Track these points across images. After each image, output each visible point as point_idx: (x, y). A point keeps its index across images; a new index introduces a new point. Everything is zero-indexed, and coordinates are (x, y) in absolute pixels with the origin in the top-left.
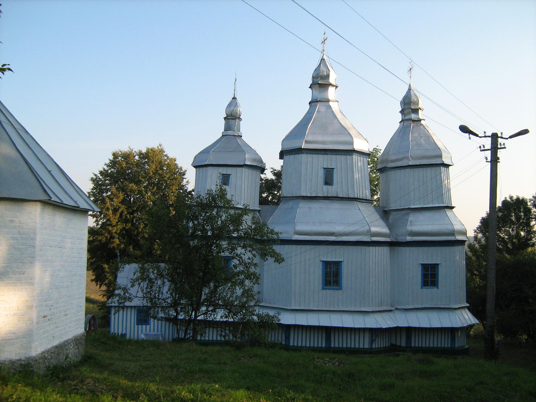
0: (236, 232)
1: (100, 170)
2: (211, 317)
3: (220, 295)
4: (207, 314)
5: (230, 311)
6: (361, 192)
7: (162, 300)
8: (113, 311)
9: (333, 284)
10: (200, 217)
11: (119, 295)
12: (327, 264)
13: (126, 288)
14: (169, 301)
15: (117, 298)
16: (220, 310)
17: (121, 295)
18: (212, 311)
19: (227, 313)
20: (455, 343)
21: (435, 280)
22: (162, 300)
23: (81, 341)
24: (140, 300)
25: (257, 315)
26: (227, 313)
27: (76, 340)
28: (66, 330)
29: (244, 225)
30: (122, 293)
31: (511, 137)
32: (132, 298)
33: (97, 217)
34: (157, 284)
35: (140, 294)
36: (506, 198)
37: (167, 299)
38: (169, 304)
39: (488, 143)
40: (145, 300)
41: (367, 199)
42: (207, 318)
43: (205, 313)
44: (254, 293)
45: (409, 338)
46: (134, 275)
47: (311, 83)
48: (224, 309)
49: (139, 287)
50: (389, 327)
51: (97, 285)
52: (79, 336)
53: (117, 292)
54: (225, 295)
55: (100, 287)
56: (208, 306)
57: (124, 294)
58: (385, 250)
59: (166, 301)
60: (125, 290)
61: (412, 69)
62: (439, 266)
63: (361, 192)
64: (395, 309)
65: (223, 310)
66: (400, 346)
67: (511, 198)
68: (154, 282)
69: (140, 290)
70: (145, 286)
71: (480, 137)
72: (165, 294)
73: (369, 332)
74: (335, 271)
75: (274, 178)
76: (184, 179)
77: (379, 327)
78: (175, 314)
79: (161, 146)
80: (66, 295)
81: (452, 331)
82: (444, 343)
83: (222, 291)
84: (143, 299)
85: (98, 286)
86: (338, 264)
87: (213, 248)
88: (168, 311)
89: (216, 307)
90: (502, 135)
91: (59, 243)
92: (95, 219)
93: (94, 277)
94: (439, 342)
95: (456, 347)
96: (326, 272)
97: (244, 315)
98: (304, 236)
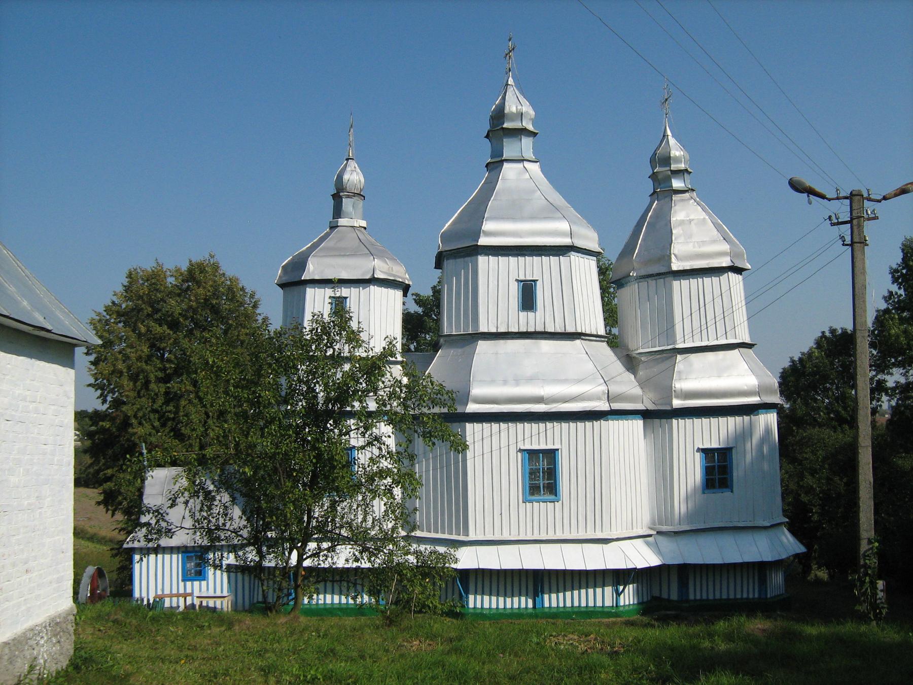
0: (371, 394)
1: (107, 305)
2: (326, 562)
3: (343, 517)
4: (319, 557)
5: (365, 550)
6: (587, 322)
7: (231, 532)
8: (137, 557)
9: (544, 491)
10: (301, 366)
11: (148, 524)
12: (532, 454)
13: (160, 511)
14: (245, 533)
15: (144, 530)
16: (343, 546)
17: (151, 524)
18: (328, 549)
19: (357, 553)
20: (766, 591)
21: (725, 476)
22: (231, 532)
23: (64, 626)
24: (188, 534)
25: (414, 553)
26: (357, 553)
27: (55, 625)
28: (28, 605)
29: (387, 380)
30: (153, 522)
31: (885, 198)
32: (172, 531)
33: (102, 389)
34: (220, 501)
35: (189, 523)
36: (823, 333)
37: (241, 529)
38: (245, 539)
39: (843, 210)
40: (198, 534)
41: (599, 334)
42: (319, 564)
43: (316, 555)
44: (407, 511)
45: (683, 585)
46: (175, 484)
47: (489, 128)
48: (352, 545)
49: (185, 509)
50: (648, 566)
51: (107, 510)
52: (59, 616)
53: (144, 519)
54: (353, 517)
55: (113, 515)
56: (319, 541)
57: (158, 521)
58: (638, 424)
59: (239, 533)
60: (158, 513)
62: (734, 451)
63: (587, 322)
64: (658, 533)
65: (351, 546)
66: (669, 600)
67: (833, 331)
68: (214, 498)
69: (187, 514)
70: (198, 508)
71: (829, 200)
72: (238, 520)
73: (613, 576)
74: (546, 467)
75: (420, 310)
76: (259, 316)
77: (630, 566)
78: (257, 559)
79: (212, 256)
80: (27, 527)
81: (761, 569)
82: (748, 591)
83: (346, 510)
84: (195, 532)
85: (110, 512)
86: (551, 455)
87: (329, 426)
88: (244, 554)
89: (337, 540)
90: (869, 195)
91: (7, 409)
92: (99, 392)
93: (101, 498)
94: (711, 590)
95: (769, 596)
97: (391, 553)
98: (492, 406)
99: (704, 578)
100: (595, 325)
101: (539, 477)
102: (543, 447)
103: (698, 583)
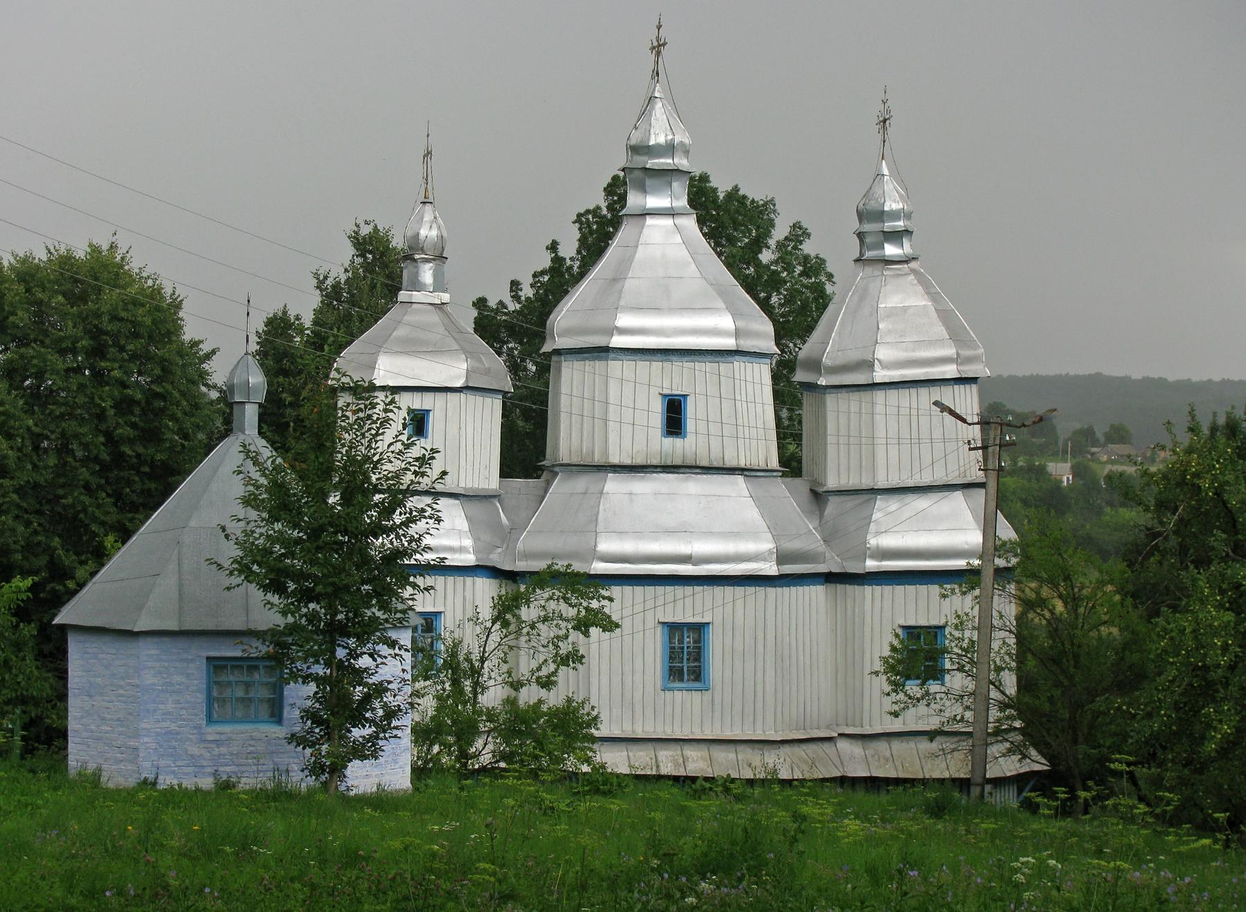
12: (673, 629)
61: (888, 122)
71: (970, 424)
86: (699, 629)
96: (671, 648)
99: (1007, 789)
100: (765, 452)
101: (682, 658)
102: (690, 620)
103: (1003, 794)
